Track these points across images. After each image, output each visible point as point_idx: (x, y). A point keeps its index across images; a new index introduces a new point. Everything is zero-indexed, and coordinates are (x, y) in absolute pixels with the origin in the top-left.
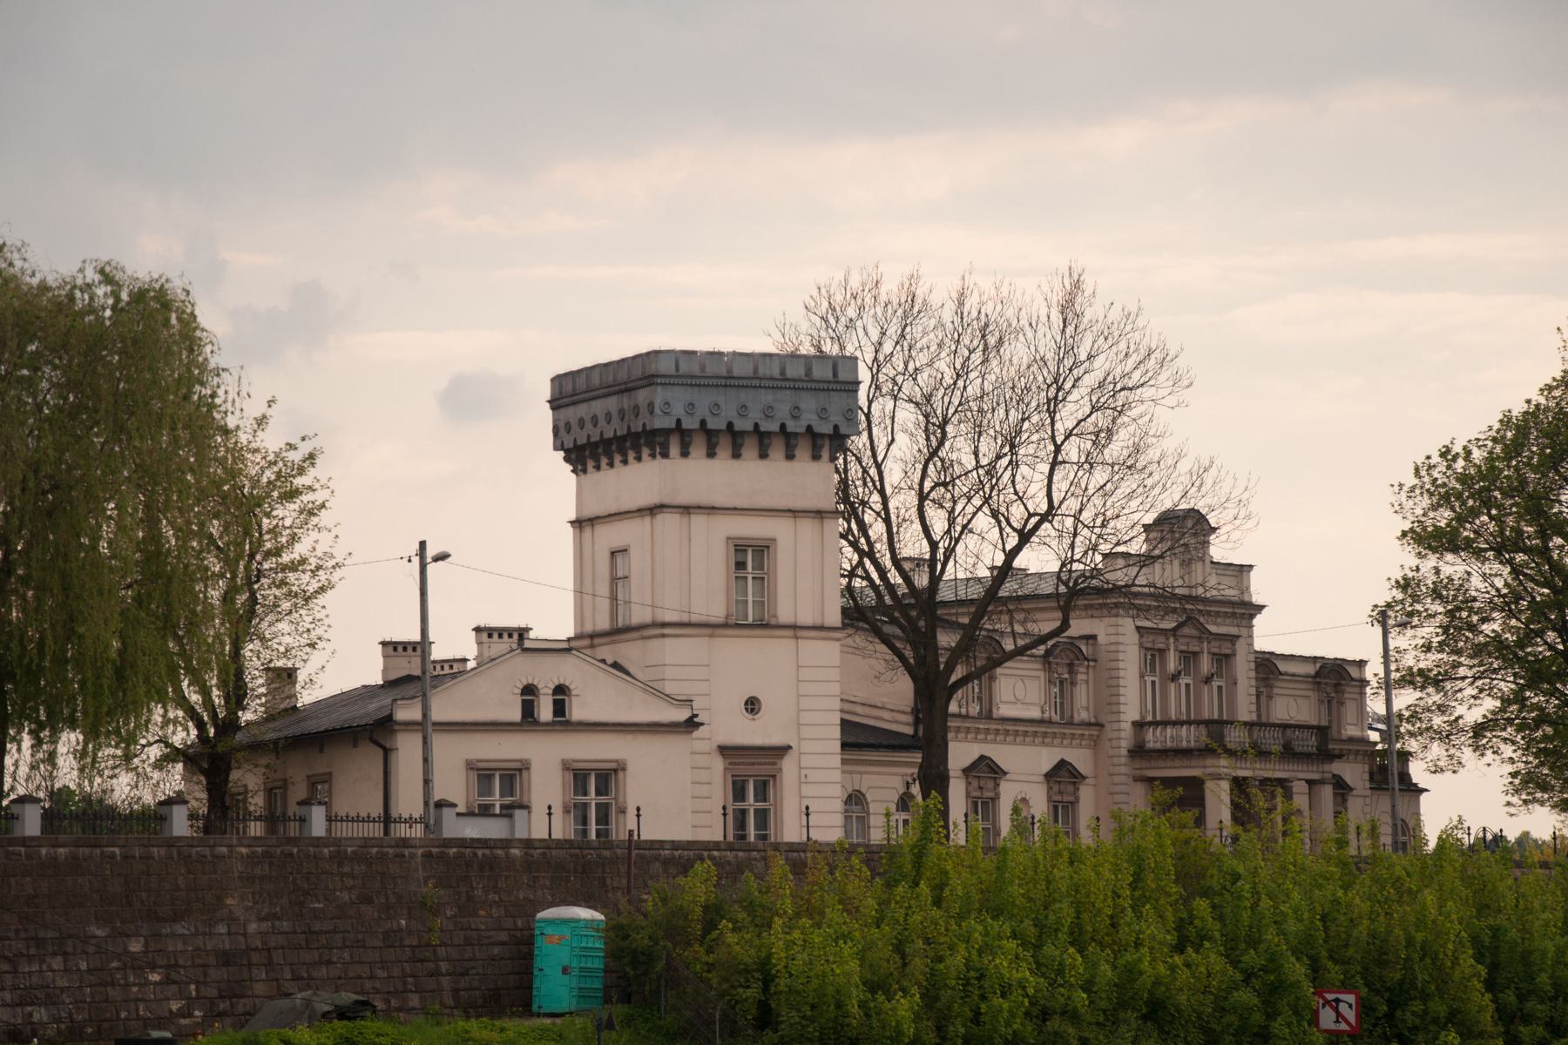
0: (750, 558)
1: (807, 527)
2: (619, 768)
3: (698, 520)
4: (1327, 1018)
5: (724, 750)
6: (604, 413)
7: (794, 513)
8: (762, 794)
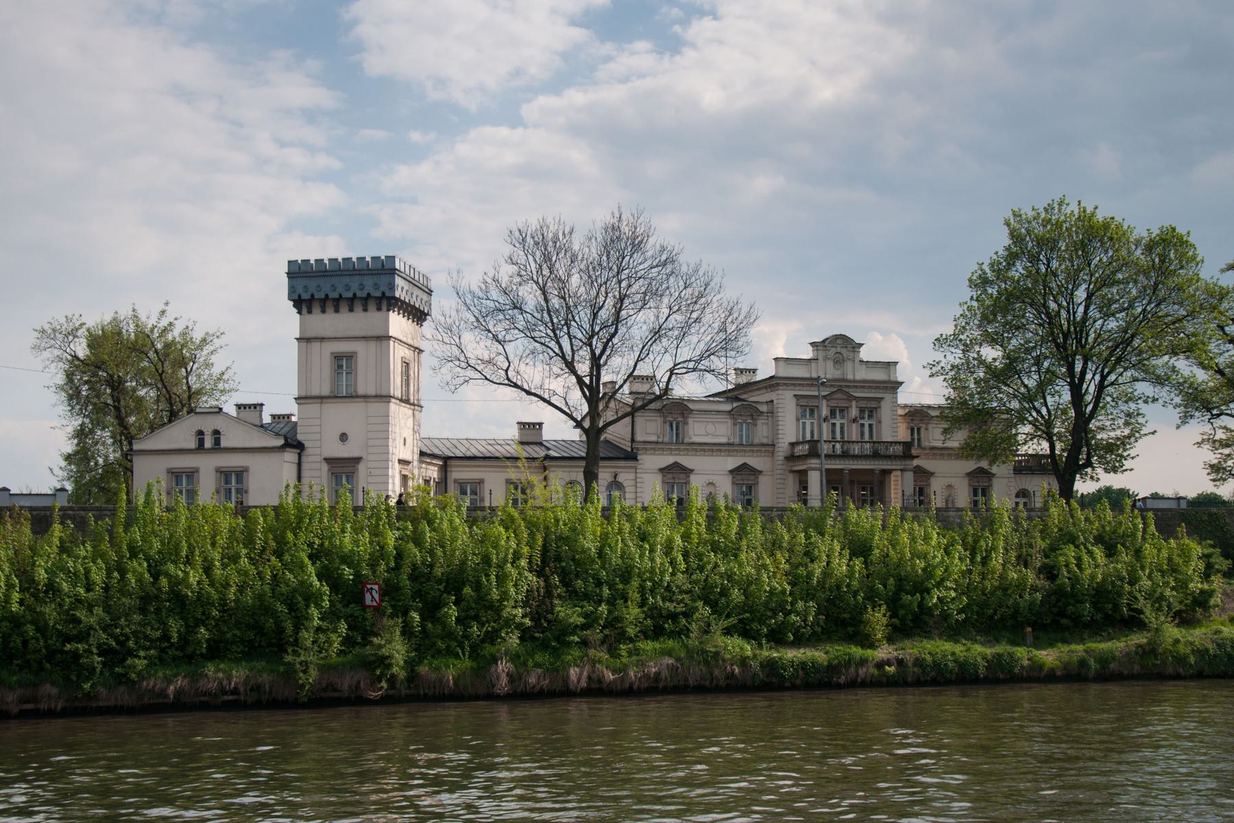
2: (246, 470)
5: (327, 460)
7: (365, 338)
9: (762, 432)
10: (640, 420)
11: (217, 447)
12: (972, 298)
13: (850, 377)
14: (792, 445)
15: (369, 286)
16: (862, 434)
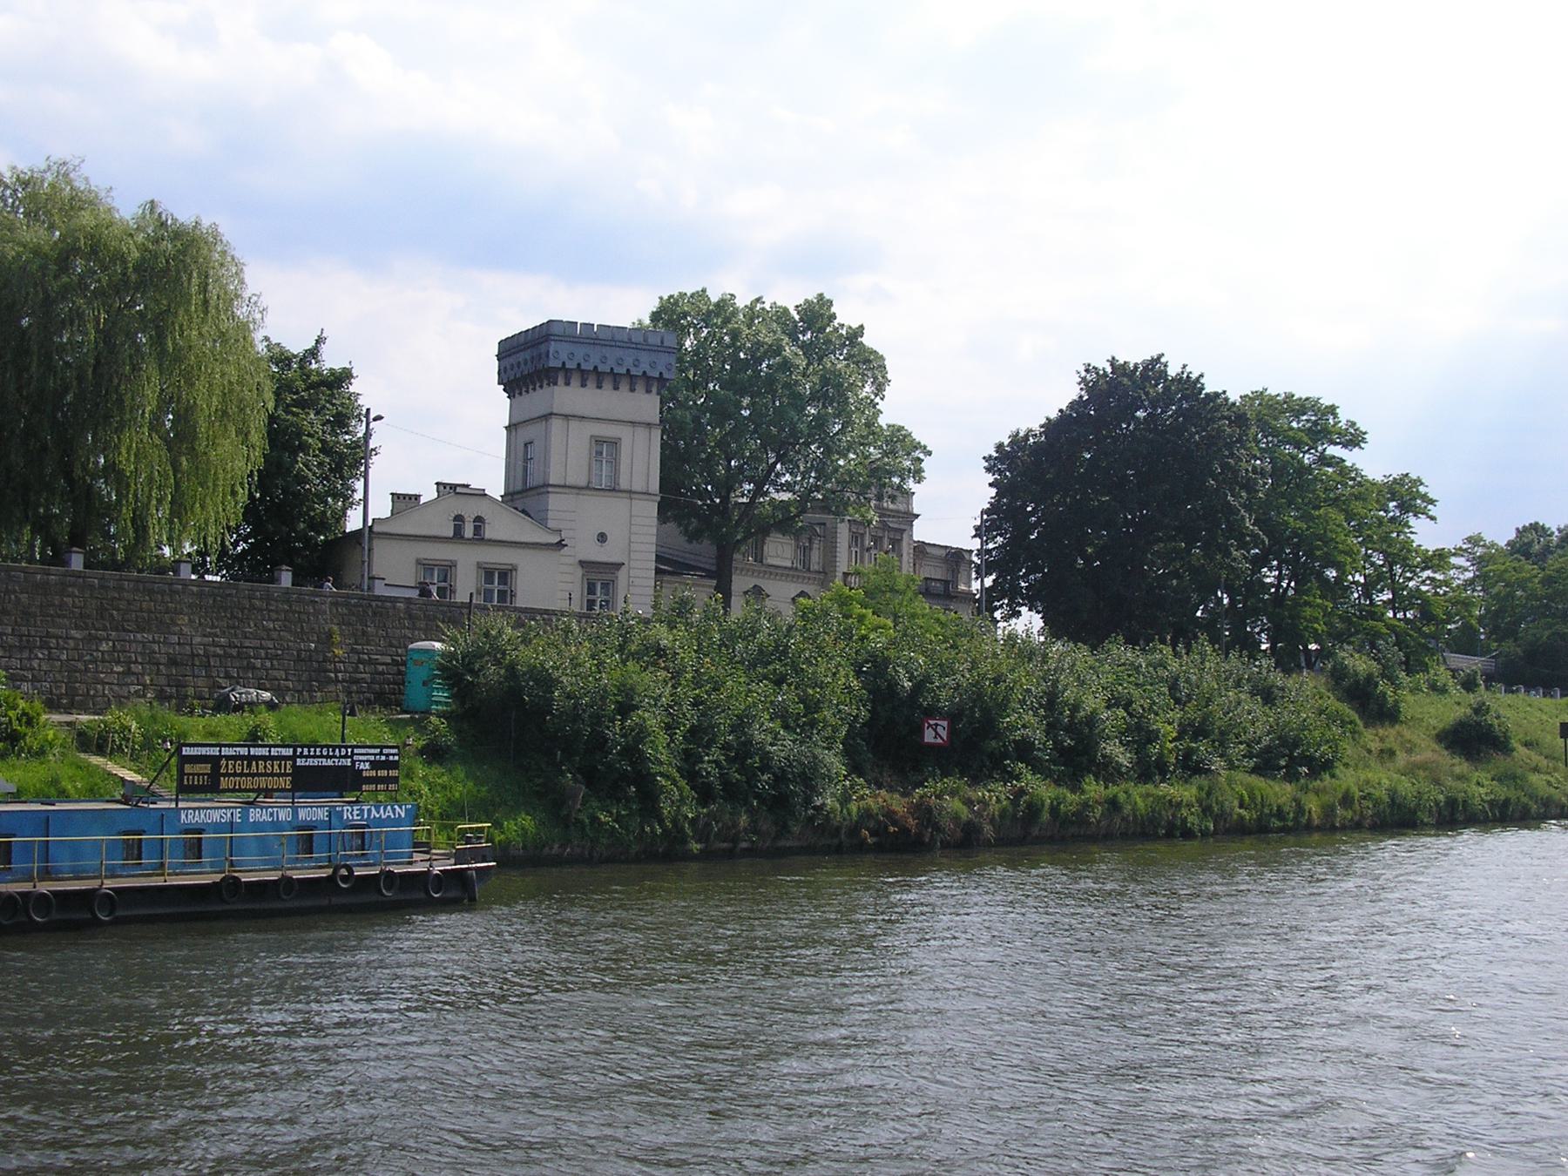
0: (605, 448)
1: (641, 433)
2: (514, 569)
3: (574, 424)
4: (929, 736)
5: (582, 563)
8: (605, 586)
11: (479, 538)
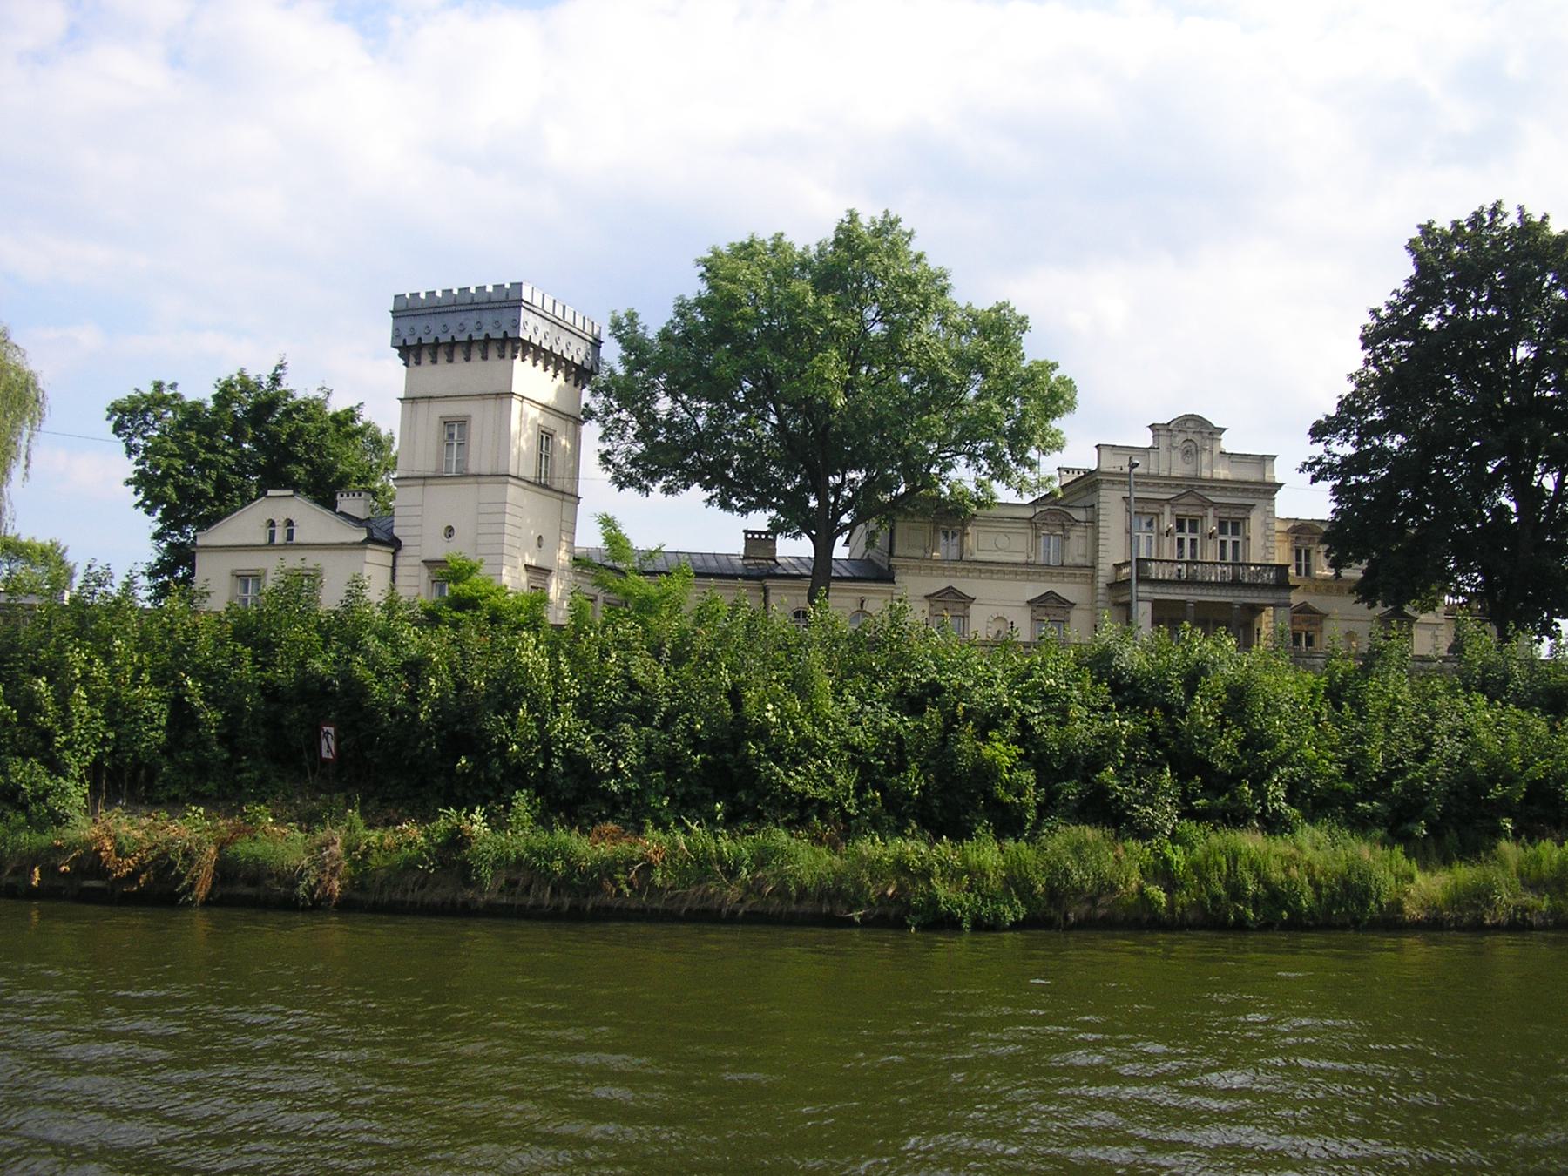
5: (429, 563)
6: (435, 330)
9: (1076, 549)
10: (901, 527)
11: (290, 544)
12: (1367, 362)
13: (1206, 474)
14: (1118, 567)
15: (490, 325)
16: (1223, 556)
